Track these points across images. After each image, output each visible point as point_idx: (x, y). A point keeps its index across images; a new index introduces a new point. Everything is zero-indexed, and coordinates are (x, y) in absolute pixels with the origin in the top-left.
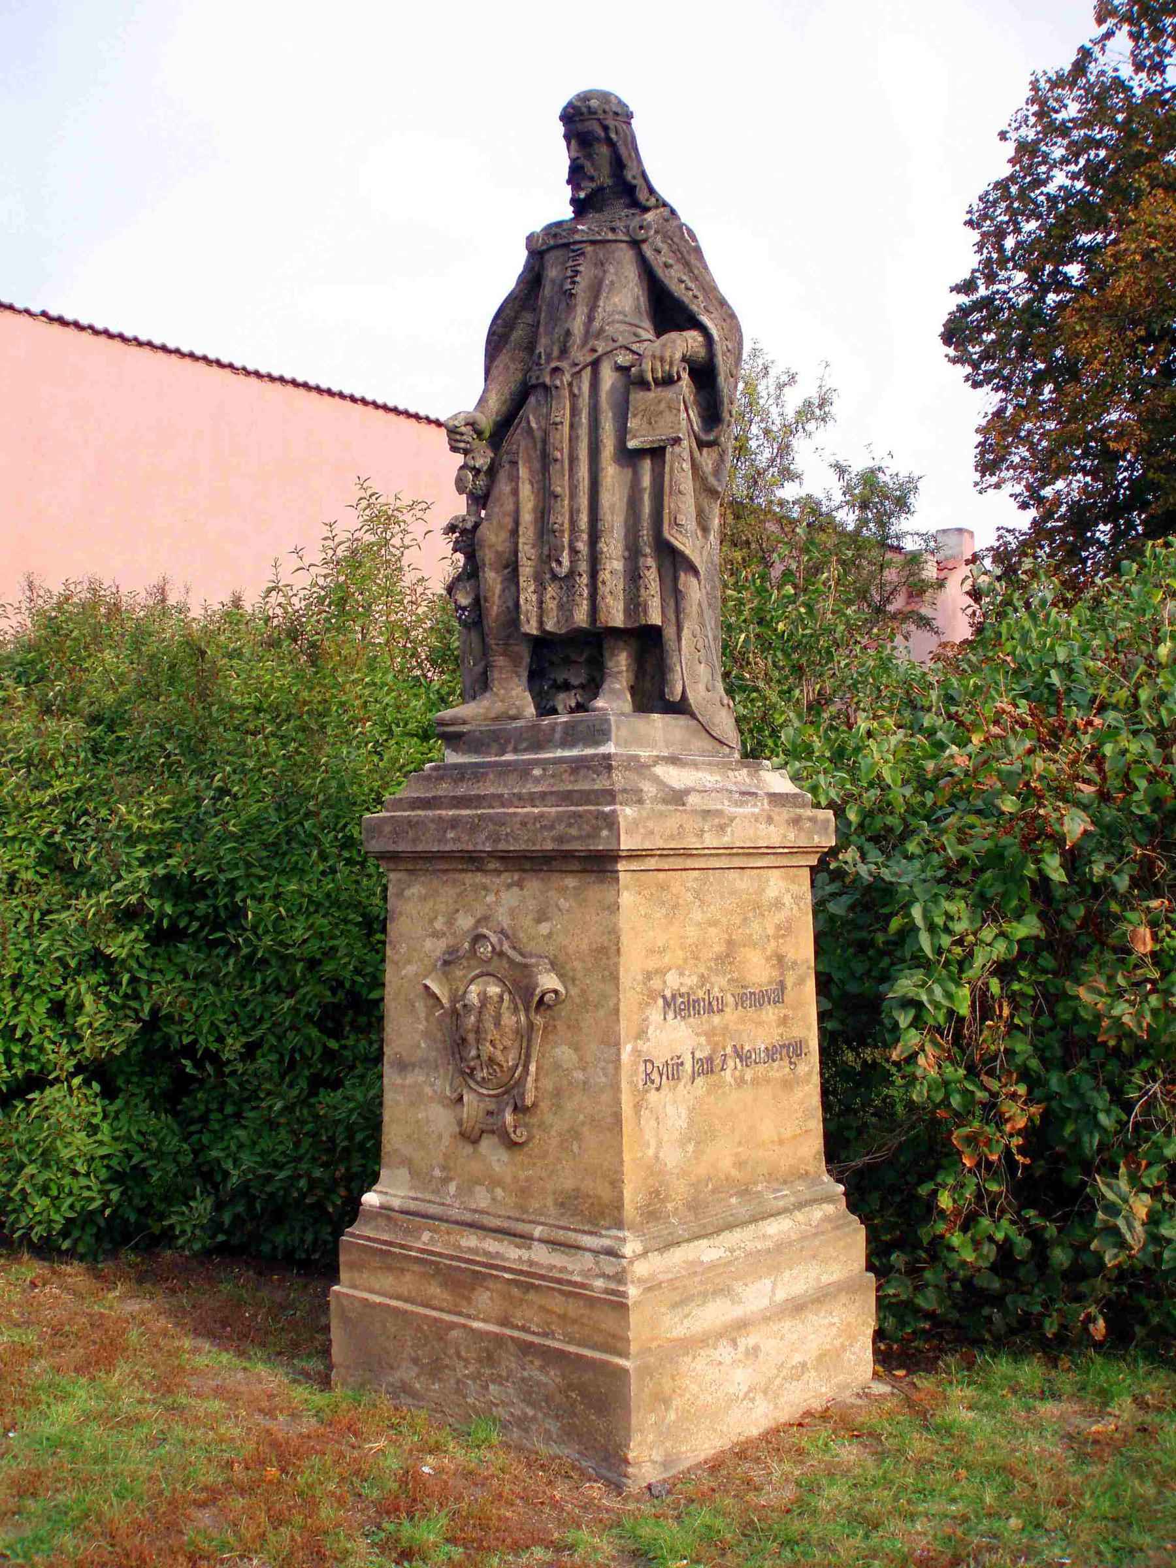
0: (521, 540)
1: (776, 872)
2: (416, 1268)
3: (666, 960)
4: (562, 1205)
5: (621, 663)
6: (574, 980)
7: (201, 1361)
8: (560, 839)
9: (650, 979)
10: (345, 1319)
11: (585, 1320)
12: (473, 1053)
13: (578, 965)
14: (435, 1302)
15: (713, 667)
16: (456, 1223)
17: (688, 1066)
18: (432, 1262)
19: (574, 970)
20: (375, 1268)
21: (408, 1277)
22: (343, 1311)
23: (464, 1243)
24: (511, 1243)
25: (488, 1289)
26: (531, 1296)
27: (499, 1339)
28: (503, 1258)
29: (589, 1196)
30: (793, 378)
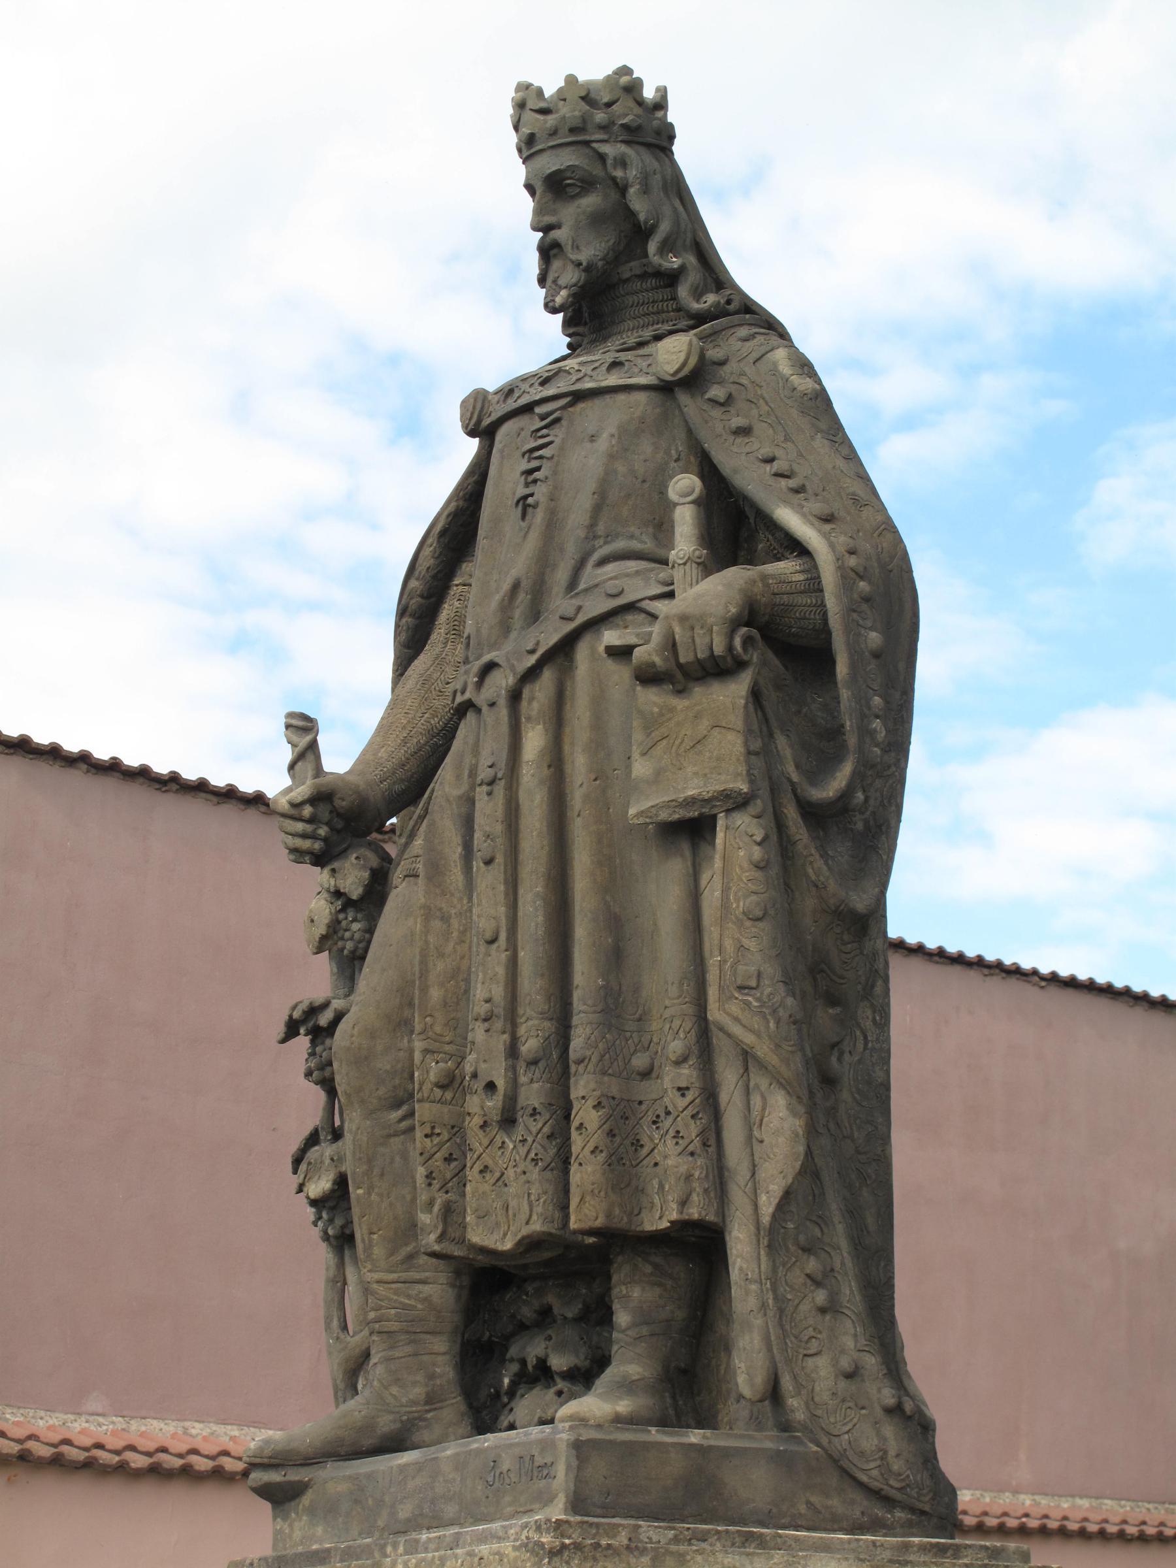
5: (634, 1299)
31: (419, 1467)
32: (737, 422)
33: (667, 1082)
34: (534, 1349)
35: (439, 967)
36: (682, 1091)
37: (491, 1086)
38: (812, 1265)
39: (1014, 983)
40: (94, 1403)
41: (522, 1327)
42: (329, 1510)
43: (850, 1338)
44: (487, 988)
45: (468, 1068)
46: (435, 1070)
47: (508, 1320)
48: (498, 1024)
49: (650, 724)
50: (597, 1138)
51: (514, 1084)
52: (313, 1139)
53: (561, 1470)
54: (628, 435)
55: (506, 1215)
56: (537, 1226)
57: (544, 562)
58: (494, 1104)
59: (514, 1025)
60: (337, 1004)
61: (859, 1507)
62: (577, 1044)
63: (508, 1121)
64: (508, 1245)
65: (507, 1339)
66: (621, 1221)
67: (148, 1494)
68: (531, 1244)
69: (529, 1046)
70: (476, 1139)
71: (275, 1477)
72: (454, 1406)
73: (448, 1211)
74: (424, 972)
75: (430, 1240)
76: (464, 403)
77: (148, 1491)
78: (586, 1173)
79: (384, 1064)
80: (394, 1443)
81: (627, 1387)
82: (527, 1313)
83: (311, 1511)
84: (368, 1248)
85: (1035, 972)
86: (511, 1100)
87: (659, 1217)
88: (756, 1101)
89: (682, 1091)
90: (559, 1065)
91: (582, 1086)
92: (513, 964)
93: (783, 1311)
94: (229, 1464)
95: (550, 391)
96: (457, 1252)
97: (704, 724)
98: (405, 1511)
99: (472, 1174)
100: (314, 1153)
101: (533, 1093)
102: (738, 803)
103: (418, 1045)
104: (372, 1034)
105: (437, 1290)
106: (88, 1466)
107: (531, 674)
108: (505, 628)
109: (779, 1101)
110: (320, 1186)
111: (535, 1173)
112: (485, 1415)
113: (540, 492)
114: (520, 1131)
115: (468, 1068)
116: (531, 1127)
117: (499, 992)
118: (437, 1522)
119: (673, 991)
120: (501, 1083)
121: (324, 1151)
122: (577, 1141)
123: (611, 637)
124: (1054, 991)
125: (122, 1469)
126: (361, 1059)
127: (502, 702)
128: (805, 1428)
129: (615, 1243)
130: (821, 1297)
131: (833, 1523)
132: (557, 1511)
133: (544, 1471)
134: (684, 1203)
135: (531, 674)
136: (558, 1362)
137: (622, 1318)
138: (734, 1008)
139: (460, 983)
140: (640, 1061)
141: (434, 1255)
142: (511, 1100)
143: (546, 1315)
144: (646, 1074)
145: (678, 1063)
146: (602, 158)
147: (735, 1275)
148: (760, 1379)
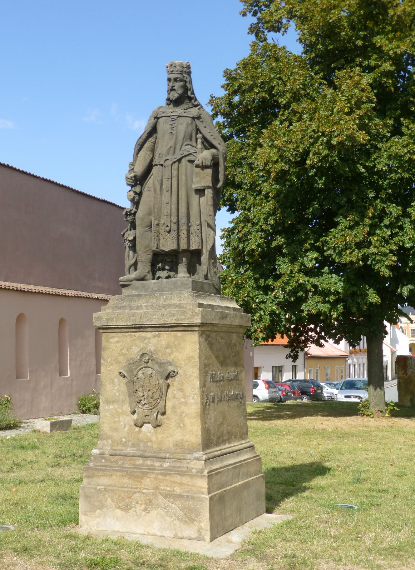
0: (37, 477)
2: (119, 473)
6: (181, 367)
7: (188, 390)
8: (177, 320)
11: (189, 483)
13: (183, 363)
14: (126, 485)
16: (134, 456)
18: (125, 471)
19: (181, 364)
20: (99, 476)
22: (85, 494)
23: (137, 463)
24: (157, 461)
25: (149, 477)
26: (167, 478)
28: (154, 466)
29: (187, 441)
30: (120, 373)
32: (205, 125)
39: (35, 179)
42: (137, 288)
44: (166, 210)
46: (156, 222)
49: (197, 174)
54: (188, 125)
55: (168, 244)
57: (175, 144)
58: (168, 229)
59: (171, 217)
63: (169, 232)
64: (167, 250)
76: (153, 112)
79: (146, 220)
85: (40, 177)
87: (193, 247)
95: (173, 114)
97: (205, 175)
101: (174, 227)
102: (209, 187)
107: (175, 162)
108: (168, 153)
113: (174, 132)
114: (171, 233)
117: (169, 212)
123: (188, 158)
124: (43, 182)
126: (143, 219)
127: (170, 166)
135: (175, 162)
139: (160, 209)
146: (184, 77)
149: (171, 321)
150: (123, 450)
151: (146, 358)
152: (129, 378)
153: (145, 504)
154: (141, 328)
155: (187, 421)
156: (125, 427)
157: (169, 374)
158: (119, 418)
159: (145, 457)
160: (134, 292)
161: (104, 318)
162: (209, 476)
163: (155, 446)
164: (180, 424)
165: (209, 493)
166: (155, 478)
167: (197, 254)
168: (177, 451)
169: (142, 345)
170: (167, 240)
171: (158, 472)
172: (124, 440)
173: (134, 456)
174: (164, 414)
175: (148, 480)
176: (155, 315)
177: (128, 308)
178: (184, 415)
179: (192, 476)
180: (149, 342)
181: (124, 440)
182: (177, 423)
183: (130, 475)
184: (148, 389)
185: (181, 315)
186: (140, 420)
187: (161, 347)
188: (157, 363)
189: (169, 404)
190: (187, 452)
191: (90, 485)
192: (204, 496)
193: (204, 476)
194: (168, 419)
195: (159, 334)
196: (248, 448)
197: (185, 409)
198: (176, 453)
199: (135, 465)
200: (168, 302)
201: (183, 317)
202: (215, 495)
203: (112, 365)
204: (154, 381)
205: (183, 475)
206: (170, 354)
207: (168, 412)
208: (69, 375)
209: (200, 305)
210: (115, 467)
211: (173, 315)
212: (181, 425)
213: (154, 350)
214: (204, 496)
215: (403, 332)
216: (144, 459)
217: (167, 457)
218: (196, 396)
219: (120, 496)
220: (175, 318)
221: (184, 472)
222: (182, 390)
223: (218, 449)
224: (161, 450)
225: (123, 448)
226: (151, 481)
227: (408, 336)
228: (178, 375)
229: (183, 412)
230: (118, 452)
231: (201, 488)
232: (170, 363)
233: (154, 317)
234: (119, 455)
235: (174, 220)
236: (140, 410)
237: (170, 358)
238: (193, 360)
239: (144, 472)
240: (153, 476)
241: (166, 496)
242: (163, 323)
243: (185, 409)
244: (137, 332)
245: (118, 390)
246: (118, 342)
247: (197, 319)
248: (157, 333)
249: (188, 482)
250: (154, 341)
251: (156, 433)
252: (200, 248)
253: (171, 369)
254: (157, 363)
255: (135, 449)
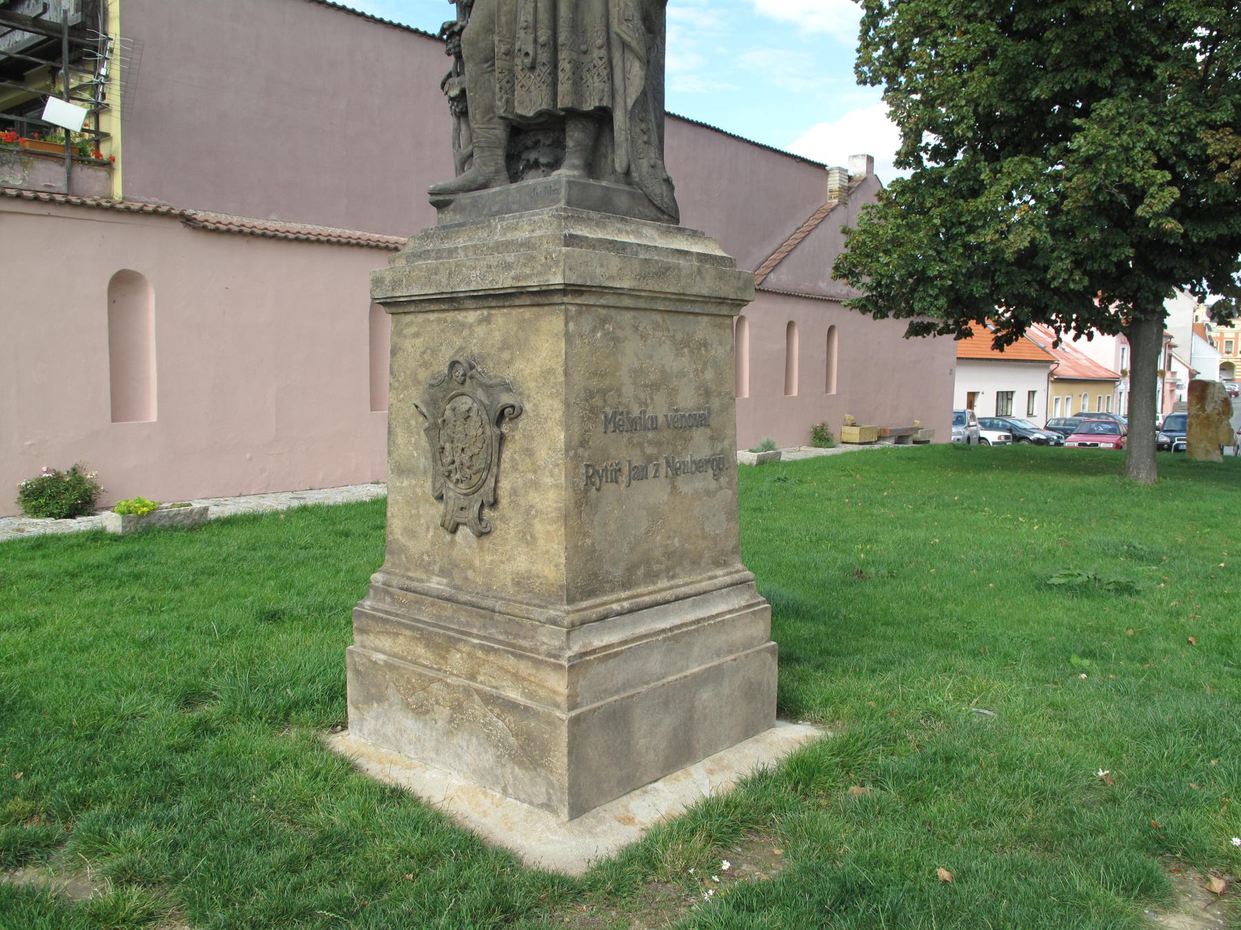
1: (706, 319)
2: (408, 633)
3: (607, 383)
4: (518, 583)
5: (575, 136)
6: (529, 396)
7: (542, 454)
9: (592, 397)
10: (357, 672)
11: (532, 679)
12: (449, 459)
13: (532, 385)
15: (645, 225)
16: (438, 597)
17: (626, 470)
18: (418, 629)
21: (401, 640)
25: (459, 651)
26: (491, 658)
27: (467, 692)
29: (538, 577)
31: (501, 192)
33: (595, 55)
34: (532, 156)
35: (505, 9)
36: (601, 58)
37: (527, 54)
38: (643, 126)
40: (273, 217)
41: (527, 148)
42: (462, 210)
43: (653, 153)
44: (525, 17)
45: (517, 47)
46: (503, 48)
47: (528, 142)
48: (530, 30)
50: (569, 74)
51: (536, 53)
52: (450, 76)
53: (563, 191)
55: (531, 100)
56: (544, 107)
58: (528, 61)
60: (460, 23)
61: (653, 212)
62: (562, 38)
63: (533, 68)
64: (531, 114)
65: (520, 153)
66: (576, 106)
67: (294, 247)
68: (540, 114)
69: (542, 39)
70: (519, 75)
71: (441, 198)
72: (504, 175)
73: (507, 101)
74: (499, 11)
75: (501, 112)
77: (294, 246)
78: (564, 87)
79: (482, 45)
80: (484, 186)
81: (574, 167)
82: (529, 143)
83: (454, 210)
84: (474, 116)
86: (535, 59)
87: (590, 105)
88: (628, 64)
89: (601, 58)
90: (554, 47)
91: (563, 55)
92: (536, 7)
93: (633, 142)
94: (322, 238)
96: (511, 117)
98: (495, 208)
99: (517, 87)
100: (450, 80)
101: (544, 56)
103: (496, 38)
104: (478, 34)
105: (500, 132)
106: (274, 237)
109: (637, 64)
110: (454, 92)
111: (544, 87)
112: (514, 177)
114: (537, 71)
115: (517, 47)
116: (543, 71)
117: (530, 18)
118: (509, 211)
119: (598, 21)
120: (531, 53)
121: (455, 80)
122: (561, 75)
125: (286, 238)
126: (473, 43)
128: (638, 184)
129: (573, 114)
130: (645, 138)
131: (646, 217)
132: (562, 204)
133: (556, 191)
134: (601, 100)
136: (543, 160)
137: (570, 143)
138: (624, 28)
140: (583, 48)
141: (502, 118)
142: (535, 59)
143: (537, 144)
144: (585, 53)
145: (600, 48)
147: (616, 128)
148: (624, 165)
149: (505, 281)
150: (422, 581)
151: (463, 373)
152: (431, 420)
153: (451, 708)
154: (452, 301)
155: (539, 527)
156: (428, 529)
157: (502, 412)
158: (418, 508)
159: (457, 602)
160: (459, 218)
161: (388, 279)
162: (571, 667)
163: (479, 580)
164: (525, 534)
165: (571, 708)
166: (469, 654)
167: (602, 118)
168: (519, 598)
169: (458, 342)
170: (529, 91)
171: (476, 641)
172: (426, 557)
173: (438, 597)
174: (494, 504)
175: (458, 656)
176: (475, 268)
177: (433, 254)
178: (533, 512)
179: (537, 663)
180: (471, 335)
181: (426, 557)
182: (519, 532)
183: (427, 639)
184: (461, 446)
185: (525, 265)
186: (449, 517)
187: (493, 346)
188: (481, 385)
189: (505, 484)
190: (536, 602)
191: (364, 647)
192: (558, 713)
193: (561, 667)
194: (503, 519)
195: (489, 315)
196: (729, 586)
197: (534, 498)
198: (515, 601)
199: (439, 617)
200: (509, 236)
201: (528, 271)
202: (594, 710)
203: (406, 387)
204: (474, 429)
205: (520, 657)
206: (509, 363)
207: (504, 502)
208: (153, 416)
209: (570, 240)
210: (403, 617)
211: (508, 267)
212: (527, 537)
213: (479, 354)
214: (558, 713)
215: (1212, 344)
216: (455, 606)
217: (497, 609)
218: (556, 470)
219: (408, 681)
220: (513, 273)
221: (524, 649)
222: (529, 453)
223: (651, 588)
224: (489, 589)
225: (424, 576)
226: (462, 659)
227: (1221, 351)
228: (523, 416)
229: (532, 507)
230: (414, 584)
231: (555, 692)
232: (507, 387)
233: (474, 273)
234: (415, 592)
235: (543, 36)
236: (451, 494)
237: (508, 375)
238: (552, 380)
239: (450, 637)
240: (466, 649)
241: (491, 700)
242: (489, 286)
243: (534, 498)
244: (448, 310)
245: (416, 446)
246: (416, 335)
247: (555, 273)
248: (485, 312)
249: (530, 675)
250: (480, 331)
251: (481, 549)
252: (606, 103)
253: (506, 399)
254: (481, 385)
255: (445, 581)
